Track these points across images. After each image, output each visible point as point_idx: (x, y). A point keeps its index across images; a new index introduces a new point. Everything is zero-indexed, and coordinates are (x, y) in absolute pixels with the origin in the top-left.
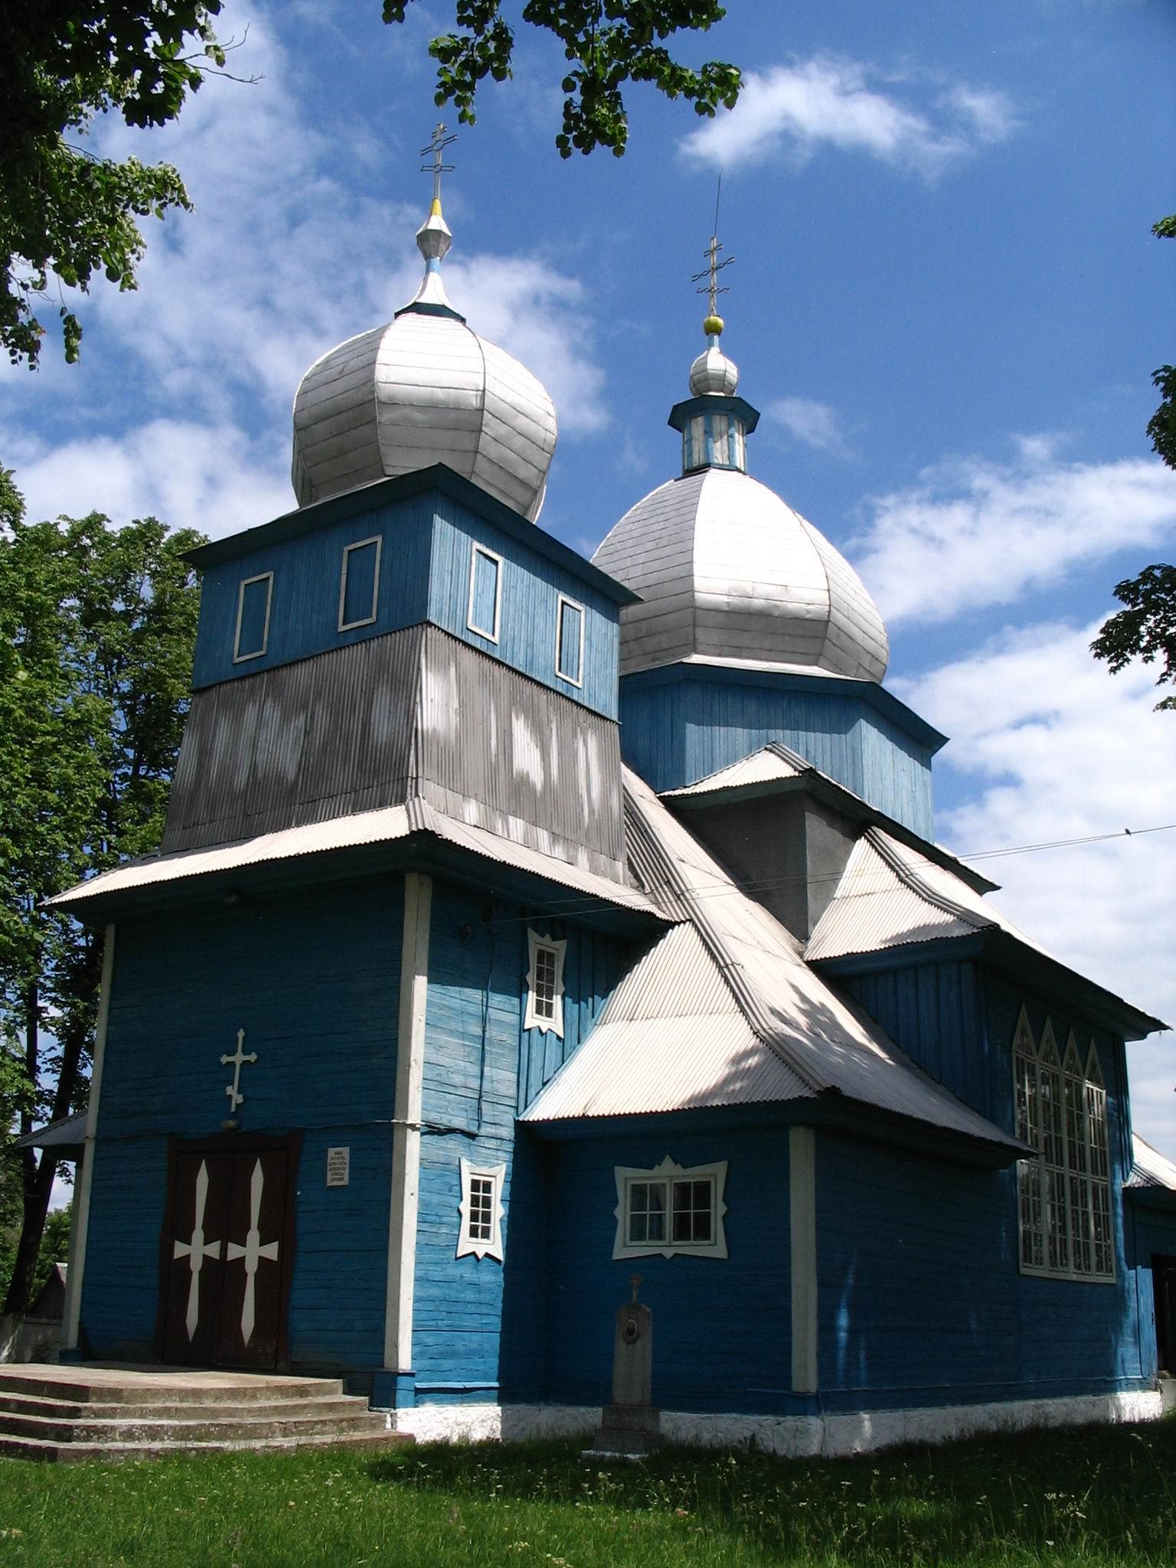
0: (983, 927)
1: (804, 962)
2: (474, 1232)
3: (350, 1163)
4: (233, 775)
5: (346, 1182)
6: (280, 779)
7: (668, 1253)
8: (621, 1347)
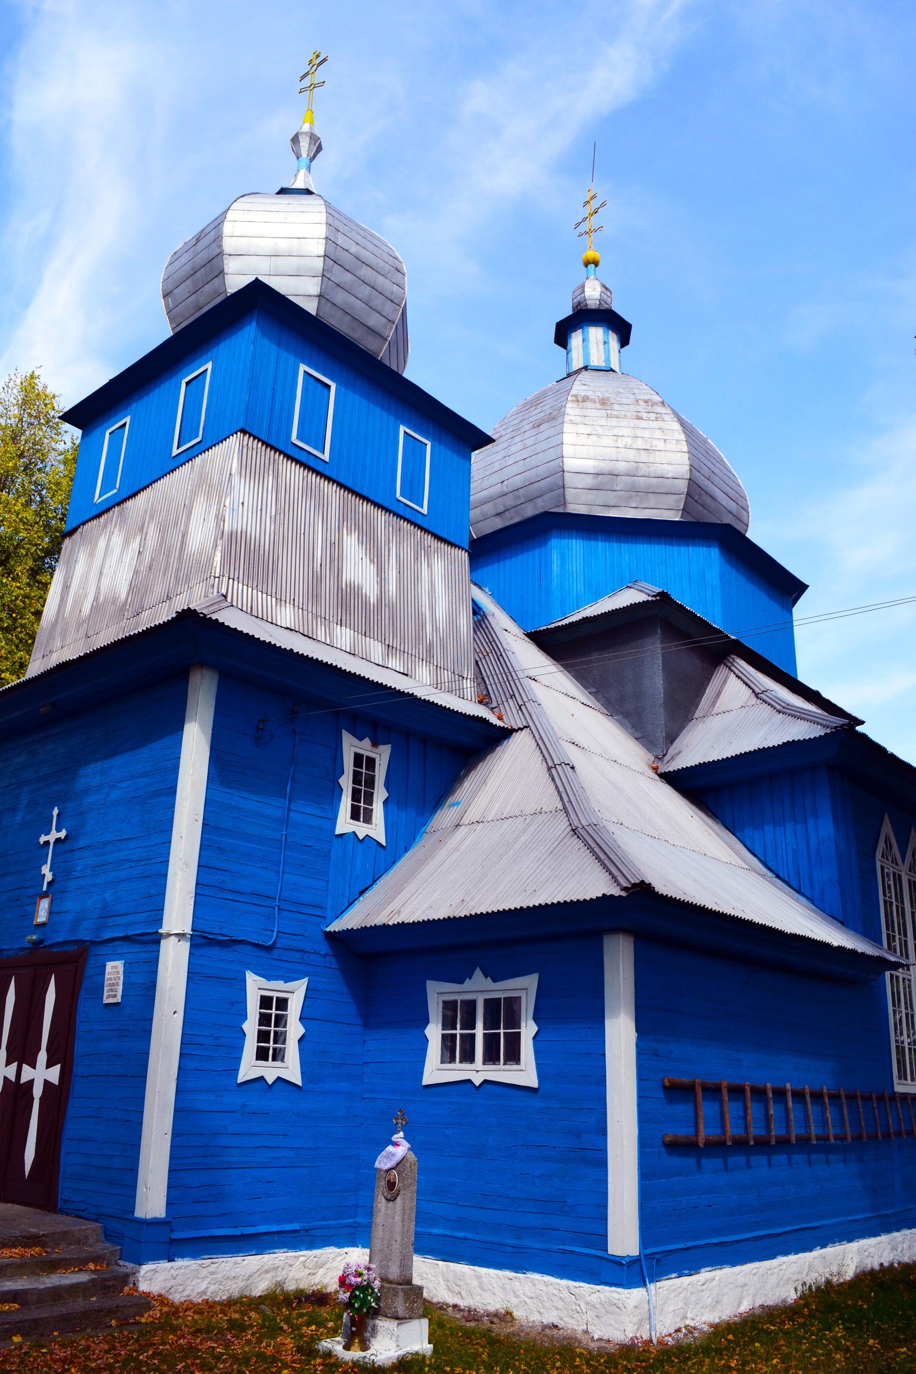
0: (837, 727)
1: (658, 775)
2: (262, 1054)
4: (83, 603)
5: (118, 999)
6: (114, 601)
8: (381, 1203)
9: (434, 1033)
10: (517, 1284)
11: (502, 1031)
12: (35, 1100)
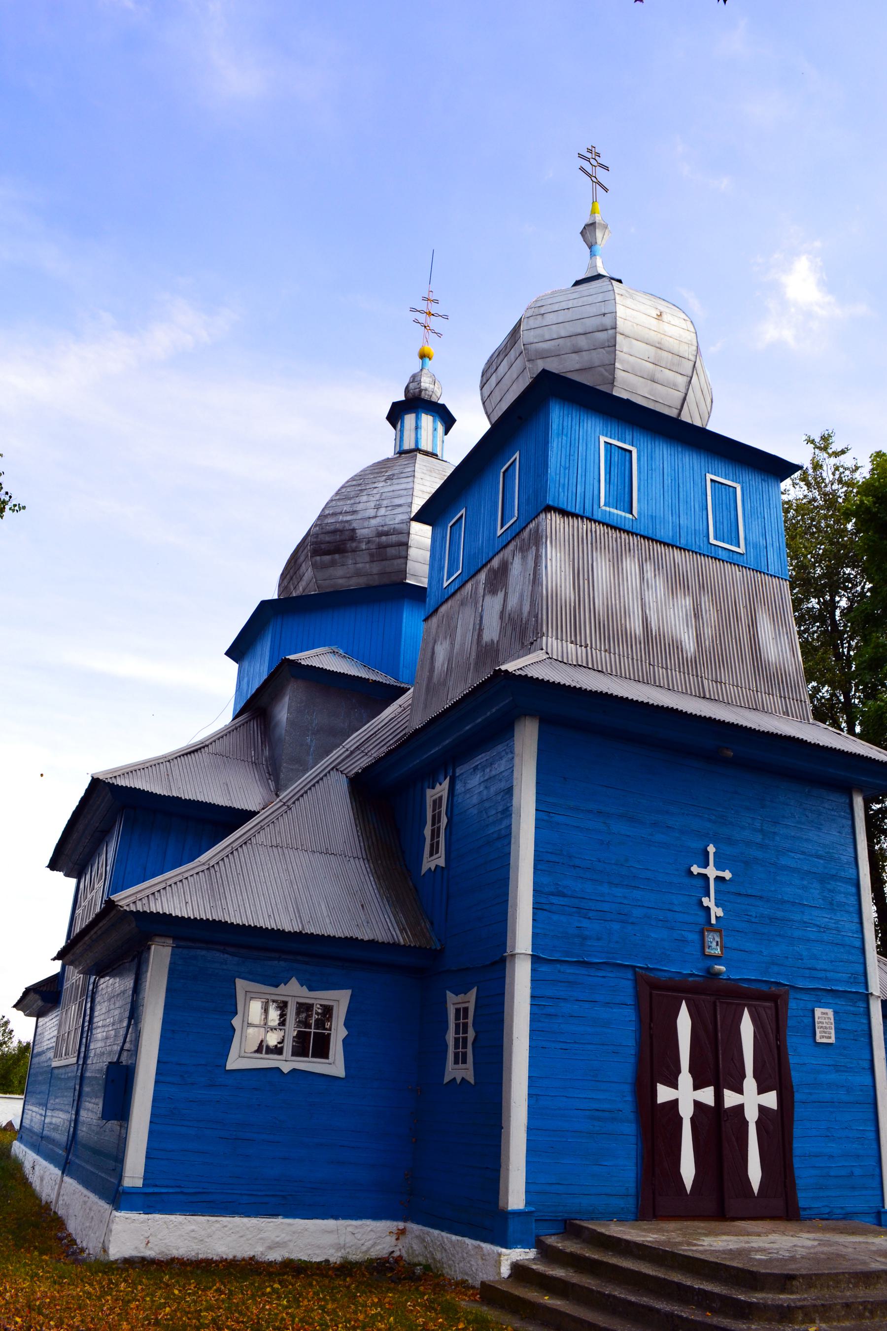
5: (832, 1040)
6: (678, 646)
7: (286, 1068)
12: (750, 1124)
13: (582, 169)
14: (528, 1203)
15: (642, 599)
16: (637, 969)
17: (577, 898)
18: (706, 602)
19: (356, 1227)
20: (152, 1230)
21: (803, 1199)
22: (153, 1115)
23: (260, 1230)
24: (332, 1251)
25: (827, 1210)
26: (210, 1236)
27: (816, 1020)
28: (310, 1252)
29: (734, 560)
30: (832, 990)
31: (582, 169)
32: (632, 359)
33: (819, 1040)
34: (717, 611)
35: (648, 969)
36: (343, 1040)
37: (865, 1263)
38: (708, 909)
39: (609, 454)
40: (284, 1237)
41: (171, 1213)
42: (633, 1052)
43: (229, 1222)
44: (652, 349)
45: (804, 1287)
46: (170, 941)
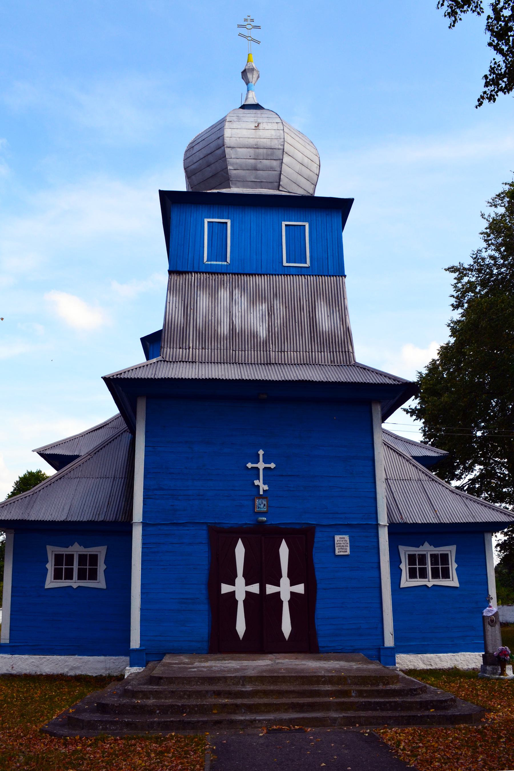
3: (350, 543)
5: (348, 552)
6: (254, 335)
7: (75, 586)
9: (50, 567)
10: (457, 657)
11: (64, 567)
13: (240, 35)
14: (141, 645)
15: (230, 312)
16: (209, 524)
17: (172, 490)
18: (277, 304)
19: (115, 660)
20: (14, 662)
21: (322, 642)
22: (11, 611)
23: (66, 661)
24: (103, 671)
25: (341, 647)
26: (41, 664)
27: (336, 542)
28: (92, 671)
29: (301, 272)
30: (348, 524)
31: (240, 35)
32: (238, 161)
33: (337, 553)
34: (286, 307)
35: (215, 523)
36: (104, 571)
37: (26, 670)
38: (258, 486)
39: (211, 228)
40: (77, 664)
41: (84, 655)
42: (207, 568)
43: (50, 658)
44: (251, 151)
45: (167, 683)
46: (13, 531)
